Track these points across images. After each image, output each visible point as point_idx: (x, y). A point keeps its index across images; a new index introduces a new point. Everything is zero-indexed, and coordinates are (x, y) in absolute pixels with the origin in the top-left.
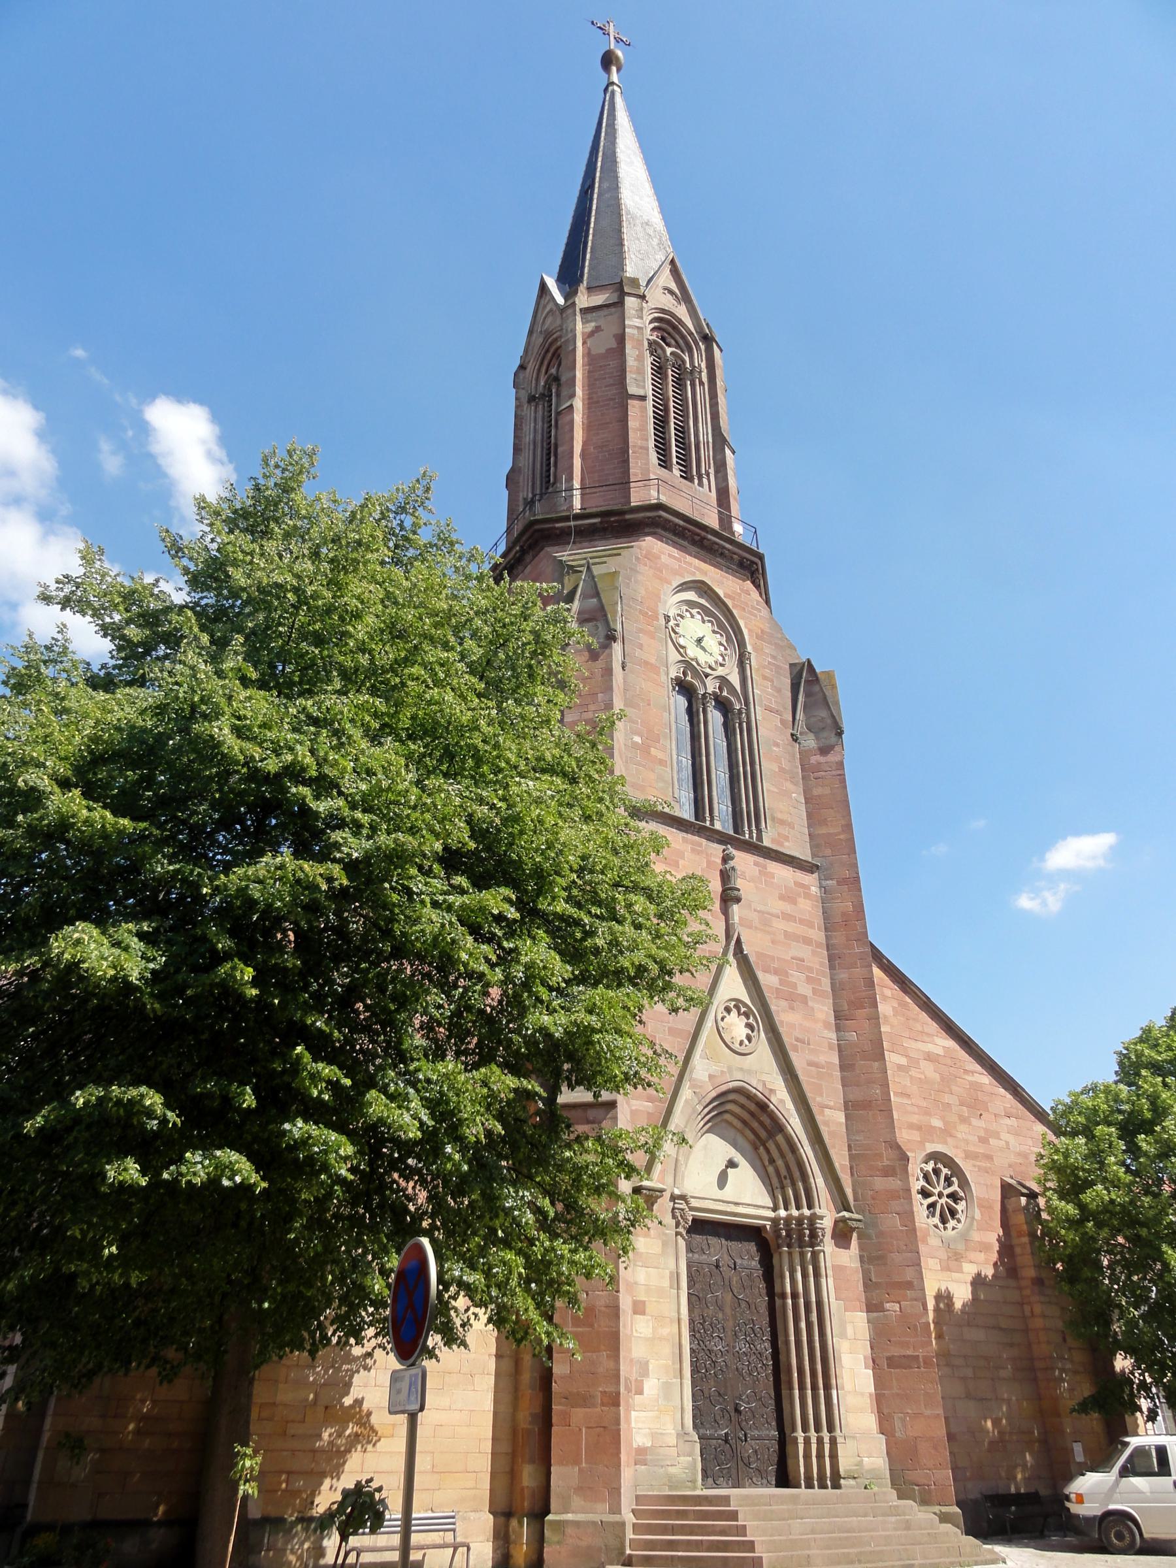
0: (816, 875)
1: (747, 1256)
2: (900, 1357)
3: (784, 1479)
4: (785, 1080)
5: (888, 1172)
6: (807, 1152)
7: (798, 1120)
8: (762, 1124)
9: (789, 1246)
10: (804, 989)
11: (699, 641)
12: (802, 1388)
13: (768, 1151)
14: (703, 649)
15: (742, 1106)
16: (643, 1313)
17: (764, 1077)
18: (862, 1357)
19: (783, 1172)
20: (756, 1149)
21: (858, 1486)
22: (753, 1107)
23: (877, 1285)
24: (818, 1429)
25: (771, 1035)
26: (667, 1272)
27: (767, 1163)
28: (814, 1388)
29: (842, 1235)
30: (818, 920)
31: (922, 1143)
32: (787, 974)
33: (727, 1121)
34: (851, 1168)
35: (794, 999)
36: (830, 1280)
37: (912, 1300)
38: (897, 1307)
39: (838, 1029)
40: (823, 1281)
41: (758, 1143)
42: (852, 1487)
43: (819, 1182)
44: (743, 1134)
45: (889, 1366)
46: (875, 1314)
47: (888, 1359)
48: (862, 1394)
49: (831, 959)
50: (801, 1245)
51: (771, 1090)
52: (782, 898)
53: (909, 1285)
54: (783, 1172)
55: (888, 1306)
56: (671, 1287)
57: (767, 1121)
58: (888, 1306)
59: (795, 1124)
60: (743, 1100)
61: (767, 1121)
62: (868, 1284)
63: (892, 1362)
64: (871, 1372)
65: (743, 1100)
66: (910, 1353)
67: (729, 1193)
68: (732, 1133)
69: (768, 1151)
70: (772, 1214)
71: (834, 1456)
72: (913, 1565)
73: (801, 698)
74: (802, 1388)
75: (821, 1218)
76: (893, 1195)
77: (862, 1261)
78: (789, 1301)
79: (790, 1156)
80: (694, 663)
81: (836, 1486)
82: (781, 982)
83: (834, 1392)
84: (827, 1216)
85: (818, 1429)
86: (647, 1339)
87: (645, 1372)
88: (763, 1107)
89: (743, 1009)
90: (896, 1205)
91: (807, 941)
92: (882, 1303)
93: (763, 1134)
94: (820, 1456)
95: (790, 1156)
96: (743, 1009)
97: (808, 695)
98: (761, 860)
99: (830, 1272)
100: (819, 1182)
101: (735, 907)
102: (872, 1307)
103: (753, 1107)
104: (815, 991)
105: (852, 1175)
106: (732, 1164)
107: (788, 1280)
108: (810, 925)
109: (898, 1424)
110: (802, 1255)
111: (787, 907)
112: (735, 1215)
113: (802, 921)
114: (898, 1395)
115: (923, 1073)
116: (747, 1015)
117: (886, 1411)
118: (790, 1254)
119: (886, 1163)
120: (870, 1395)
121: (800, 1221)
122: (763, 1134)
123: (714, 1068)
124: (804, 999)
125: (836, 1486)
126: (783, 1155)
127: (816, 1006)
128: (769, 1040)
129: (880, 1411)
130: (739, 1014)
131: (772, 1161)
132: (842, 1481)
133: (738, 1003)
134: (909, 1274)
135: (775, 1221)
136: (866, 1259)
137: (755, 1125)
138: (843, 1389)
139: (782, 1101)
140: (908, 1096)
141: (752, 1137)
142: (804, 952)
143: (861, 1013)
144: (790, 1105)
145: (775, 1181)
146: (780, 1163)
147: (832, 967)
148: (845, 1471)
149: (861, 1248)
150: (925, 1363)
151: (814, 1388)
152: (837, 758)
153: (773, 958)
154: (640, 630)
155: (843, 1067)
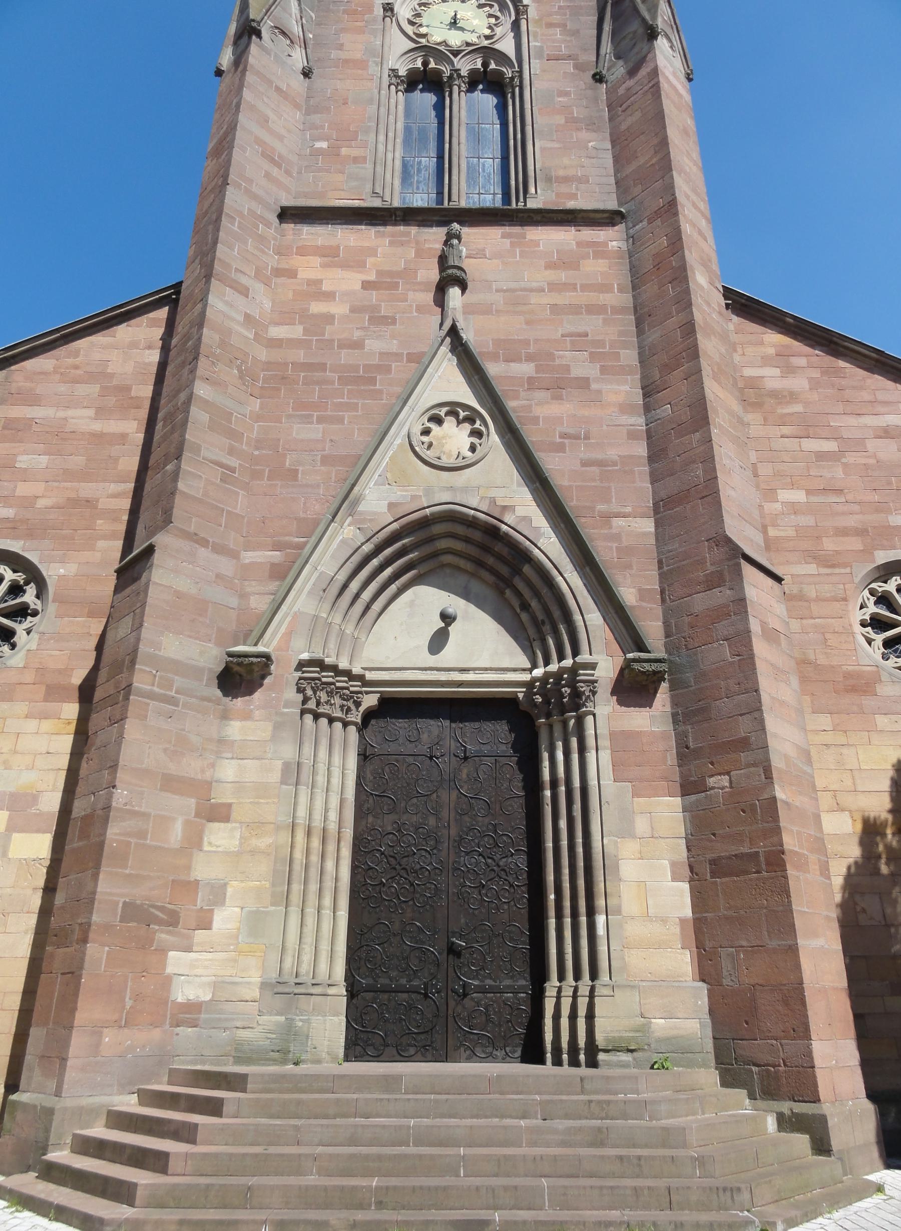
0: (621, 227)
1: (496, 735)
2: (729, 858)
3: (533, 1053)
4: (533, 492)
5: (714, 582)
6: (571, 581)
7: (554, 539)
8: (499, 557)
9: (548, 715)
10: (581, 366)
11: (454, 23)
12: (559, 917)
13: (519, 594)
14: (462, 29)
15: (467, 540)
16: (226, 819)
17: (493, 493)
18: (666, 863)
19: (540, 616)
20: (502, 593)
21: (637, 1064)
22: (477, 535)
23: (697, 753)
24: (577, 977)
25: (509, 435)
26: (279, 764)
27: (518, 610)
28: (575, 915)
29: (634, 688)
30: (619, 275)
31: (868, 552)
32: (551, 356)
33: (449, 565)
34: (662, 592)
35: (559, 384)
36: (605, 756)
37: (748, 765)
38: (725, 781)
39: (647, 408)
40: (591, 756)
41: (502, 585)
42: (625, 1065)
43: (591, 618)
44: (480, 578)
45: (714, 874)
46: (693, 798)
47: (713, 862)
48: (664, 920)
49: (639, 323)
50: (563, 710)
51: (505, 508)
52: (550, 266)
53: (743, 744)
54: (540, 616)
55: (711, 781)
56: (284, 782)
57: (505, 551)
58: (711, 781)
59: (548, 545)
60: (460, 530)
61: (505, 551)
62: (685, 754)
63: (718, 867)
64: (686, 886)
65: (460, 530)
66: (745, 849)
67: (449, 655)
68: (462, 579)
69: (519, 594)
70: (526, 677)
71: (590, 1016)
72: (485, 1223)
73: (607, 27)
74: (559, 917)
75: (593, 666)
76: (720, 614)
77: (675, 721)
78: (548, 793)
79: (544, 591)
80: (442, 48)
81: (593, 1063)
82: (538, 369)
83: (600, 920)
84: (604, 661)
85: (577, 977)
86: (227, 853)
87: (219, 894)
88: (492, 532)
89: (462, 414)
90: (723, 628)
91: (593, 309)
92: (703, 779)
93: (504, 570)
94: (573, 1016)
95: (544, 591)
96: (462, 414)
97: (614, 18)
98: (517, 230)
99: (604, 742)
100: (591, 618)
101: (454, 292)
102: (689, 787)
103: (477, 535)
104: (604, 370)
105: (663, 600)
106: (447, 618)
107: (546, 764)
108: (605, 288)
109: (726, 965)
110: (565, 723)
111: (562, 276)
112: (460, 684)
113: (584, 288)
114: (727, 918)
115: (875, 456)
116: (470, 420)
117: (708, 945)
118: (551, 726)
119: (710, 569)
120: (683, 921)
121: (558, 676)
122: (504, 570)
123: (398, 494)
124: (584, 383)
125: (593, 1063)
126: (537, 594)
127: (605, 387)
128: (507, 445)
129: (700, 945)
130: (459, 423)
131: (525, 606)
132: (601, 1056)
133: (453, 408)
134: (744, 726)
135: (529, 685)
136: (682, 716)
137: (491, 561)
138: (619, 911)
139: (527, 519)
140: (839, 491)
141: (491, 578)
142: (592, 325)
143: (678, 373)
144: (540, 521)
145: (532, 632)
146: (534, 604)
147: (640, 332)
148: (607, 1039)
149: (675, 703)
150: (768, 864)
151: (575, 915)
152: (652, 66)
153: (526, 342)
154: (343, 30)
155: (653, 457)
